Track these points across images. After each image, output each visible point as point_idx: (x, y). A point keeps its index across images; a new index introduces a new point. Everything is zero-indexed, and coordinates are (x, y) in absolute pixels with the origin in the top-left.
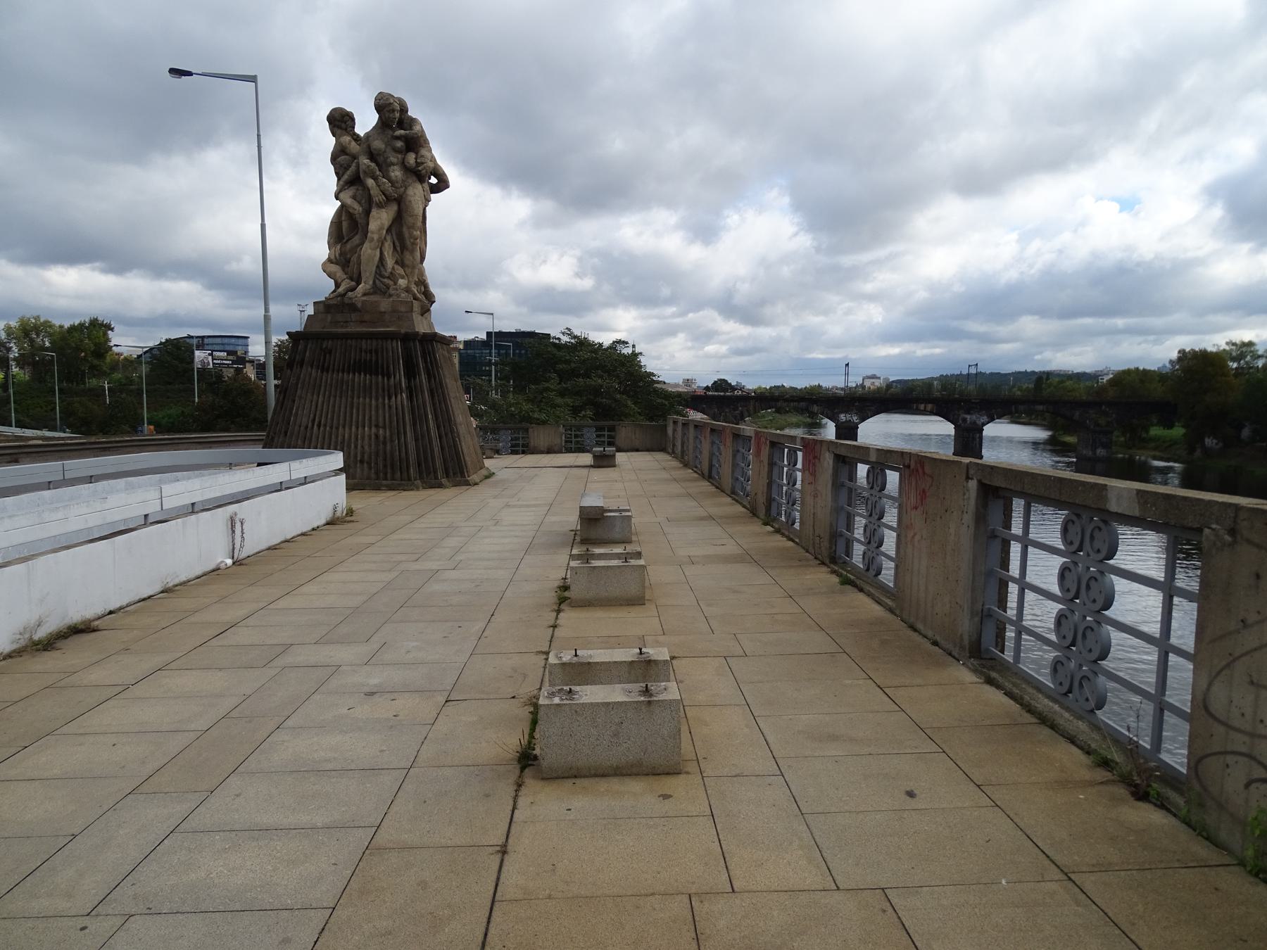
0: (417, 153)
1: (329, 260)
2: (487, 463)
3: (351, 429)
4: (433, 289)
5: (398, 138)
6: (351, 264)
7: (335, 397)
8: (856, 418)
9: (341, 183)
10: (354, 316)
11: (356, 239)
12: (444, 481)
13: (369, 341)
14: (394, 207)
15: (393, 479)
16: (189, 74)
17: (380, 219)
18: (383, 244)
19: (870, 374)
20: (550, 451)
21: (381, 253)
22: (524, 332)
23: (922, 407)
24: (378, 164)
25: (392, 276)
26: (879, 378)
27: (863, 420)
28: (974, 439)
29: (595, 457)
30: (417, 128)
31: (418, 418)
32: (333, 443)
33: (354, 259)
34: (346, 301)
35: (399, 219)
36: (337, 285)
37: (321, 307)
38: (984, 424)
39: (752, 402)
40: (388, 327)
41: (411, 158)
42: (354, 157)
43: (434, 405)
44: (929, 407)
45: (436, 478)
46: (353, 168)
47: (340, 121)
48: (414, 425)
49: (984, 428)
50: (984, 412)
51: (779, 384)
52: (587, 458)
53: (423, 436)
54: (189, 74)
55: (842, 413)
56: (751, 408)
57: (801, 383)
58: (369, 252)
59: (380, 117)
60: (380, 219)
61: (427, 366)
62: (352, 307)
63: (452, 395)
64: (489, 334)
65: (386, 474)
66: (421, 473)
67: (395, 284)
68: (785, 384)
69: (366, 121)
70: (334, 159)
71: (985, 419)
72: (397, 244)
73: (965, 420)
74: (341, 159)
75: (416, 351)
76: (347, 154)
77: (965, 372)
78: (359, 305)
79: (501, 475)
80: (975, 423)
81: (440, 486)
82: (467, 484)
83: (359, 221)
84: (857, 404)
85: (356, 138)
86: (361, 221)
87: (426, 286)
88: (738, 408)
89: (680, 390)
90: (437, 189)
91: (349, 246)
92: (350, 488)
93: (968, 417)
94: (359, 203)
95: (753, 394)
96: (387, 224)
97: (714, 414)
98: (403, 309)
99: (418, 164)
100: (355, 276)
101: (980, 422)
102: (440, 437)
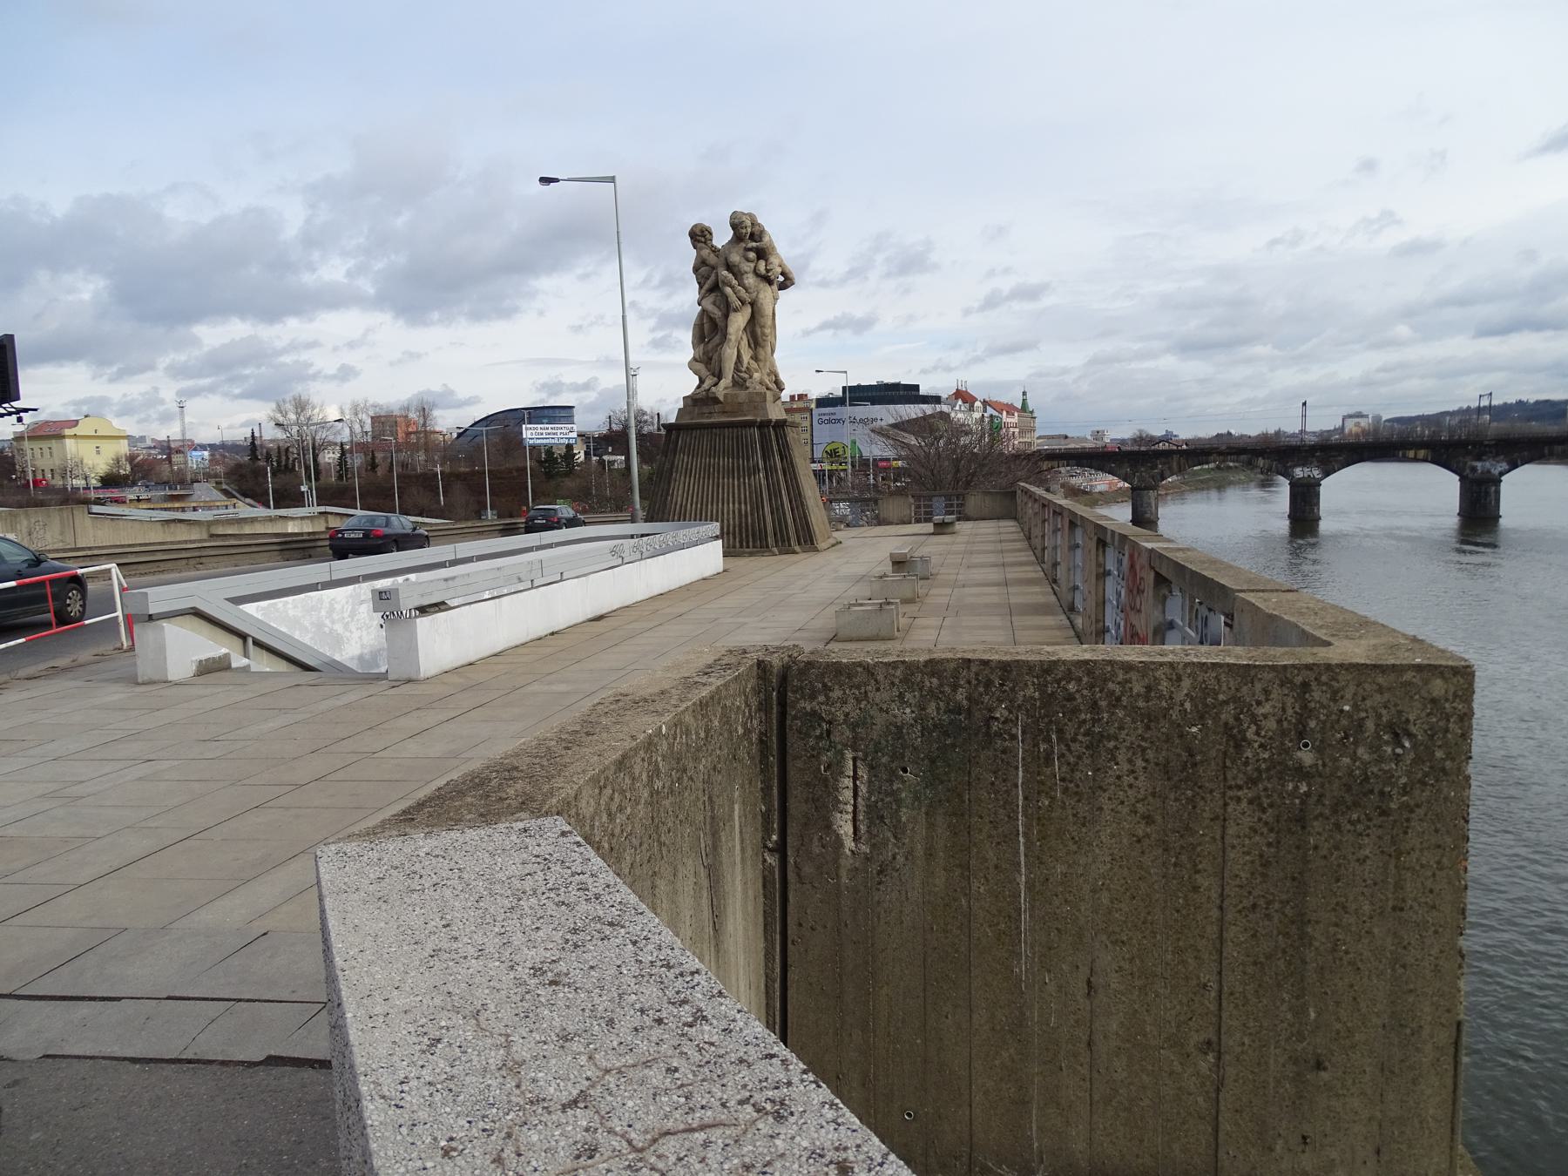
0: (766, 261)
1: (694, 359)
2: (836, 534)
3: (718, 505)
4: (782, 377)
5: (750, 249)
6: (713, 361)
7: (704, 478)
8: (1317, 472)
9: (703, 291)
10: (717, 408)
11: (717, 339)
12: (797, 548)
13: (735, 430)
14: (748, 310)
15: (754, 547)
16: (556, 180)
17: (738, 321)
18: (739, 343)
19: (1352, 411)
20: (904, 522)
21: (739, 351)
22: (887, 385)
23: (1411, 454)
24: (734, 274)
25: (748, 370)
26: (1367, 416)
27: (1327, 474)
28: (1487, 493)
29: (935, 524)
30: (766, 239)
31: (774, 493)
32: (698, 517)
33: (715, 357)
34: (711, 395)
35: (753, 322)
36: (702, 381)
37: (690, 402)
38: (1502, 474)
39: (1176, 457)
40: (745, 415)
41: (762, 266)
42: (713, 268)
43: (786, 482)
44: (1422, 453)
45: (790, 545)
46: (713, 277)
47: (699, 236)
48: (770, 500)
49: (1503, 478)
50: (1502, 457)
51: (1224, 431)
52: (929, 527)
53: (777, 509)
54: (556, 180)
55: (1299, 466)
56: (1175, 465)
57: (1253, 430)
58: (730, 353)
59: (735, 233)
60: (738, 321)
61: (779, 449)
62: (716, 400)
63: (801, 473)
64: (844, 388)
65: (748, 543)
66: (776, 542)
67: (751, 377)
68: (1233, 432)
69: (722, 237)
70: (696, 270)
71: (1505, 466)
72: (751, 341)
73: (1474, 469)
74: (702, 269)
75: (770, 436)
76: (707, 265)
77: (1474, 405)
78: (721, 399)
79: (846, 543)
80: (1489, 472)
81: (794, 552)
82: (816, 550)
83: (719, 324)
84: (1318, 454)
85: (715, 250)
86: (721, 324)
87: (776, 376)
88: (1156, 466)
89: (1088, 445)
90: (783, 287)
91: (710, 346)
92: (726, 554)
93: (1479, 465)
94: (718, 307)
95: (1184, 447)
96: (743, 326)
97: (1126, 474)
98: (758, 399)
99: (768, 271)
100: (717, 372)
101: (1495, 472)
102: (792, 510)
